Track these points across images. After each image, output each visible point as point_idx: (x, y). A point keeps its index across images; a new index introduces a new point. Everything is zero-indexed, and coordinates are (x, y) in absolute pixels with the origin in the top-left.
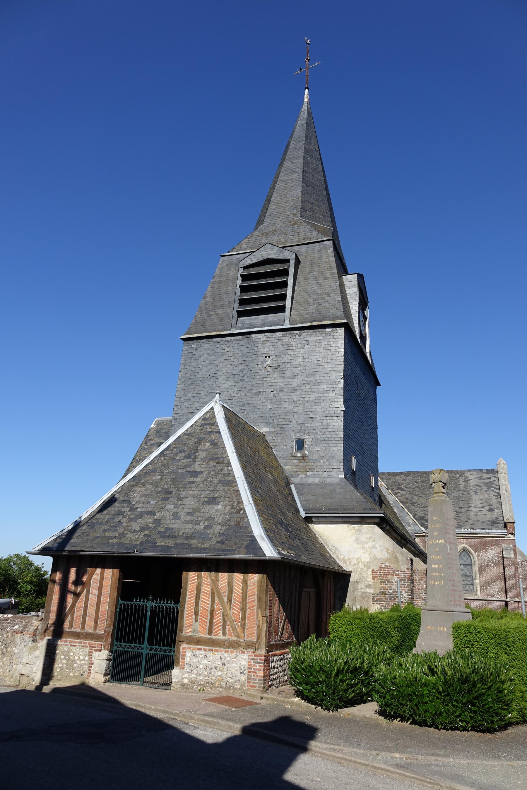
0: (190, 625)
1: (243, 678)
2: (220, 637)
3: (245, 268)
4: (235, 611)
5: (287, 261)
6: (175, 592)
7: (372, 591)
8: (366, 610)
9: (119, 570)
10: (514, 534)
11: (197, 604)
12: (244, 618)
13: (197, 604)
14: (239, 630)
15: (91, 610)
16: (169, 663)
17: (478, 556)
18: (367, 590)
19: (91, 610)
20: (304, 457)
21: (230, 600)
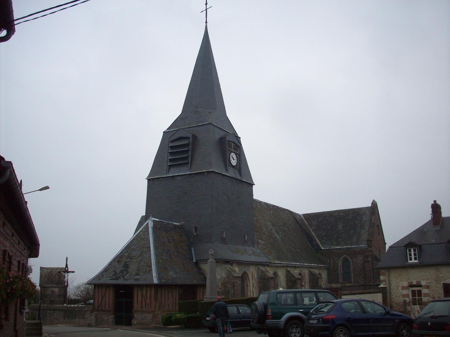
0: (136, 306)
1: (151, 321)
2: (144, 309)
3: (172, 142)
4: (148, 301)
5: (188, 138)
6: (131, 296)
7: (221, 290)
8: (420, 282)
9: (370, 205)
10: (371, 247)
11: (137, 299)
12: (151, 303)
13: (137, 299)
14: (150, 307)
15: (107, 302)
16: (132, 318)
17: (352, 261)
18: (219, 290)
19: (107, 302)
20: (197, 235)
21: (146, 298)
